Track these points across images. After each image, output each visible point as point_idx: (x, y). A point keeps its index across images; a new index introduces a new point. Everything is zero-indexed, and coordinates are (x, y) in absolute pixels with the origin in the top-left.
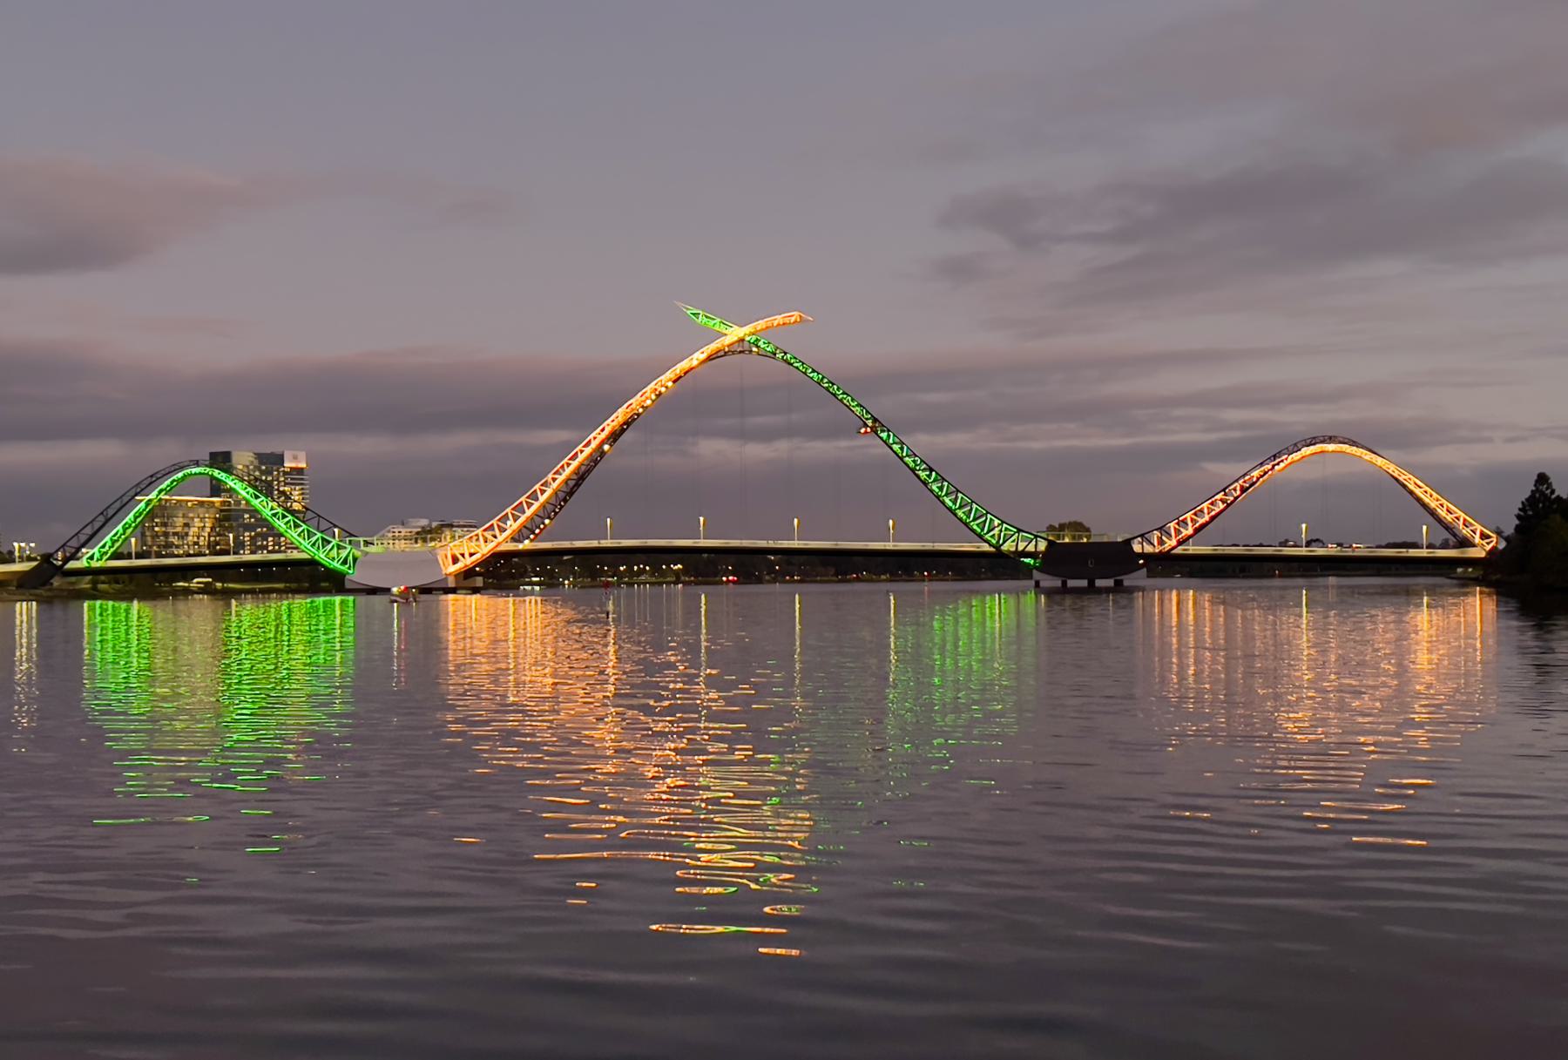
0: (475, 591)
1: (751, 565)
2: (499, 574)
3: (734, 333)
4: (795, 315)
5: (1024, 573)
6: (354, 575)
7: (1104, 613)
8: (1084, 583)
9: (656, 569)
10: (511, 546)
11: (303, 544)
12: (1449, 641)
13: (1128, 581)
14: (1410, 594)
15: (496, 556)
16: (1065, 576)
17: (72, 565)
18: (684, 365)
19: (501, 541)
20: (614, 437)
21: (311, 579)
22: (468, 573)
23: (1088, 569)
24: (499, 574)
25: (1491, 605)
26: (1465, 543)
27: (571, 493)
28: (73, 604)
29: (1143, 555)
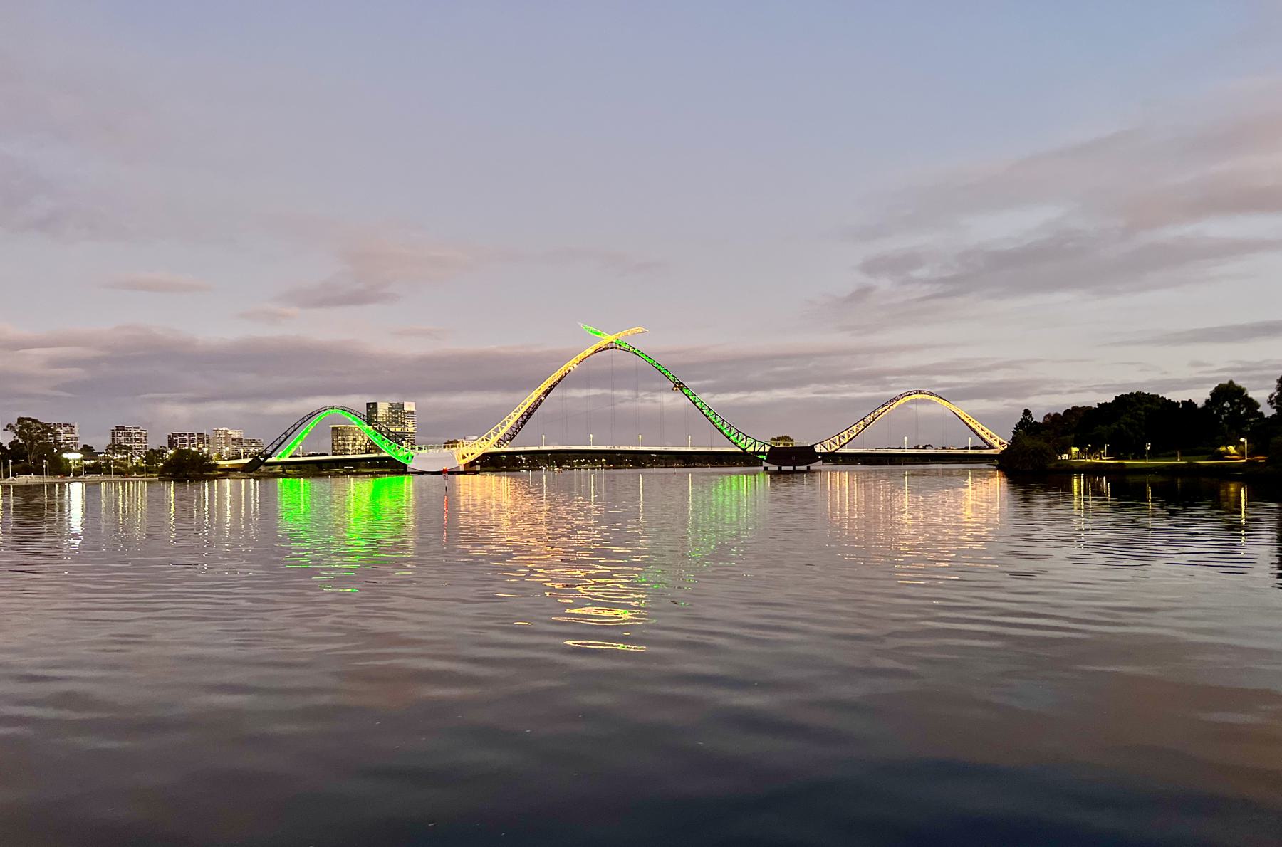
0: (476, 473)
1: (616, 459)
2: (490, 463)
3: (607, 339)
4: (640, 330)
5: (757, 463)
6: (411, 465)
7: (800, 489)
8: (791, 468)
9: (593, 462)
10: (495, 450)
11: (389, 450)
12: (985, 497)
13: (813, 467)
14: (964, 475)
15: (485, 455)
16: (780, 465)
17: (269, 460)
18: (582, 355)
19: (489, 447)
20: (547, 393)
21: (398, 468)
22: (473, 463)
23: (790, 460)
24: (490, 463)
25: (1004, 480)
26: (991, 447)
27: (525, 422)
28: (271, 481)
29: (820, 454)
